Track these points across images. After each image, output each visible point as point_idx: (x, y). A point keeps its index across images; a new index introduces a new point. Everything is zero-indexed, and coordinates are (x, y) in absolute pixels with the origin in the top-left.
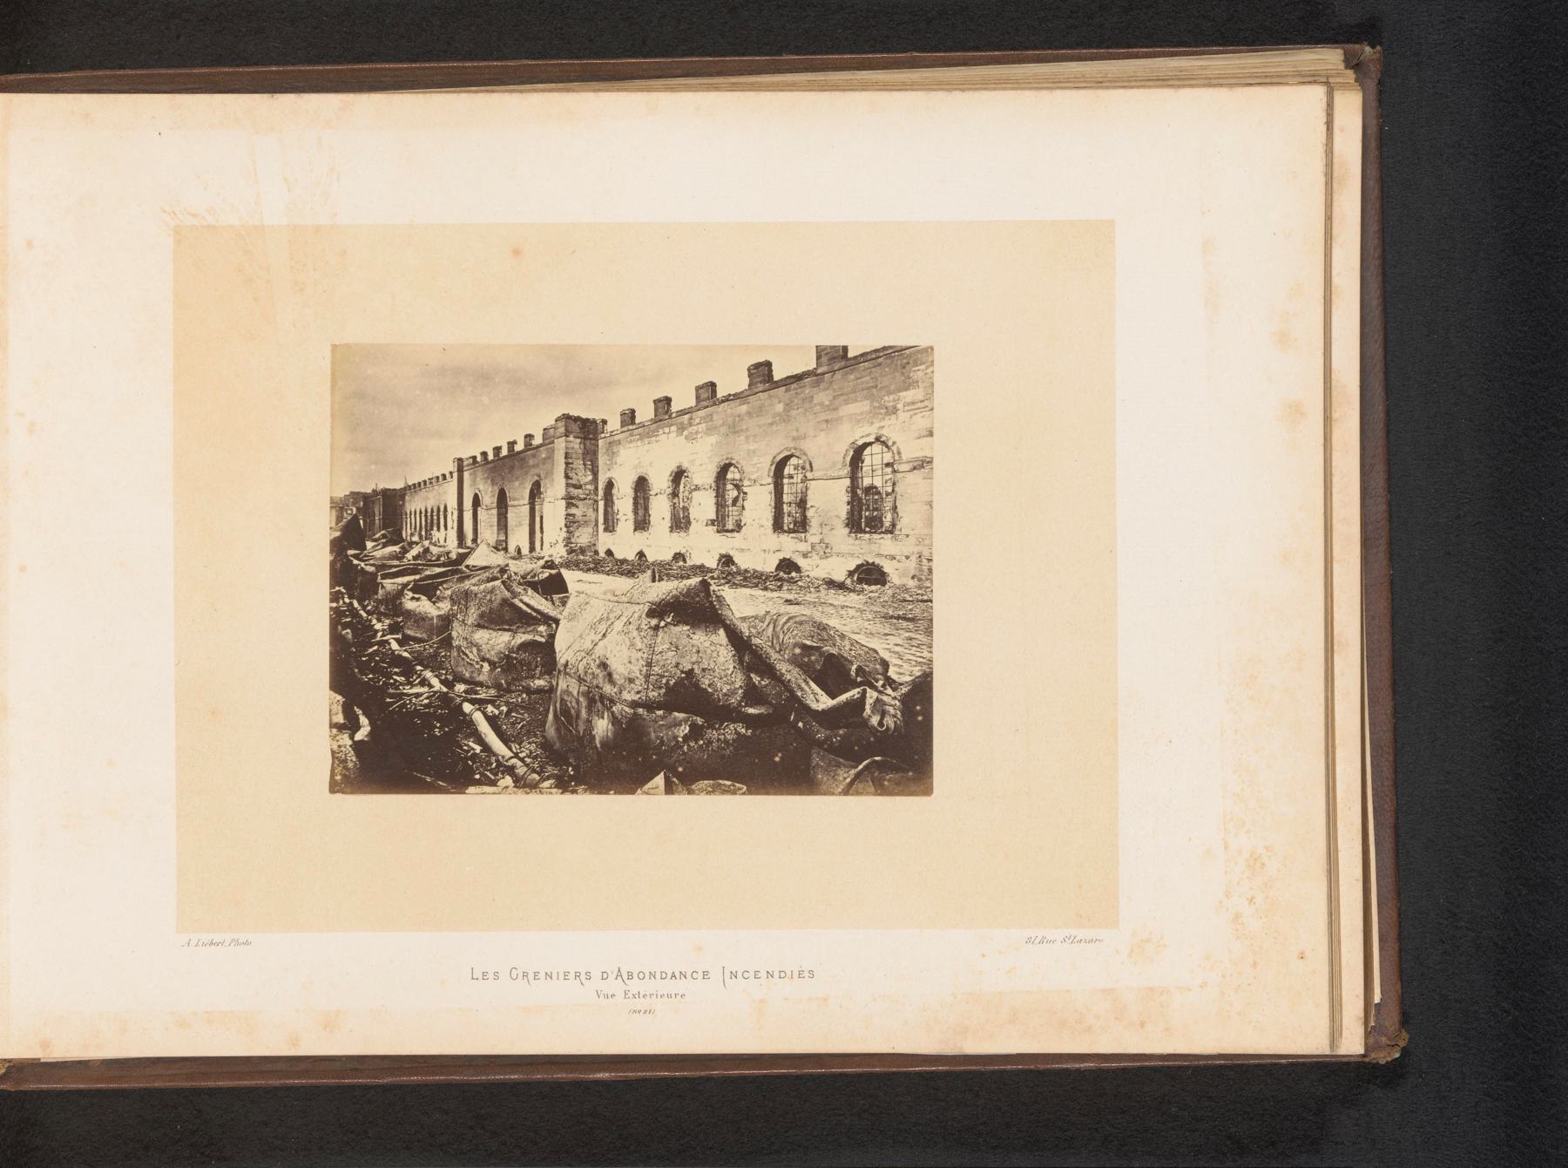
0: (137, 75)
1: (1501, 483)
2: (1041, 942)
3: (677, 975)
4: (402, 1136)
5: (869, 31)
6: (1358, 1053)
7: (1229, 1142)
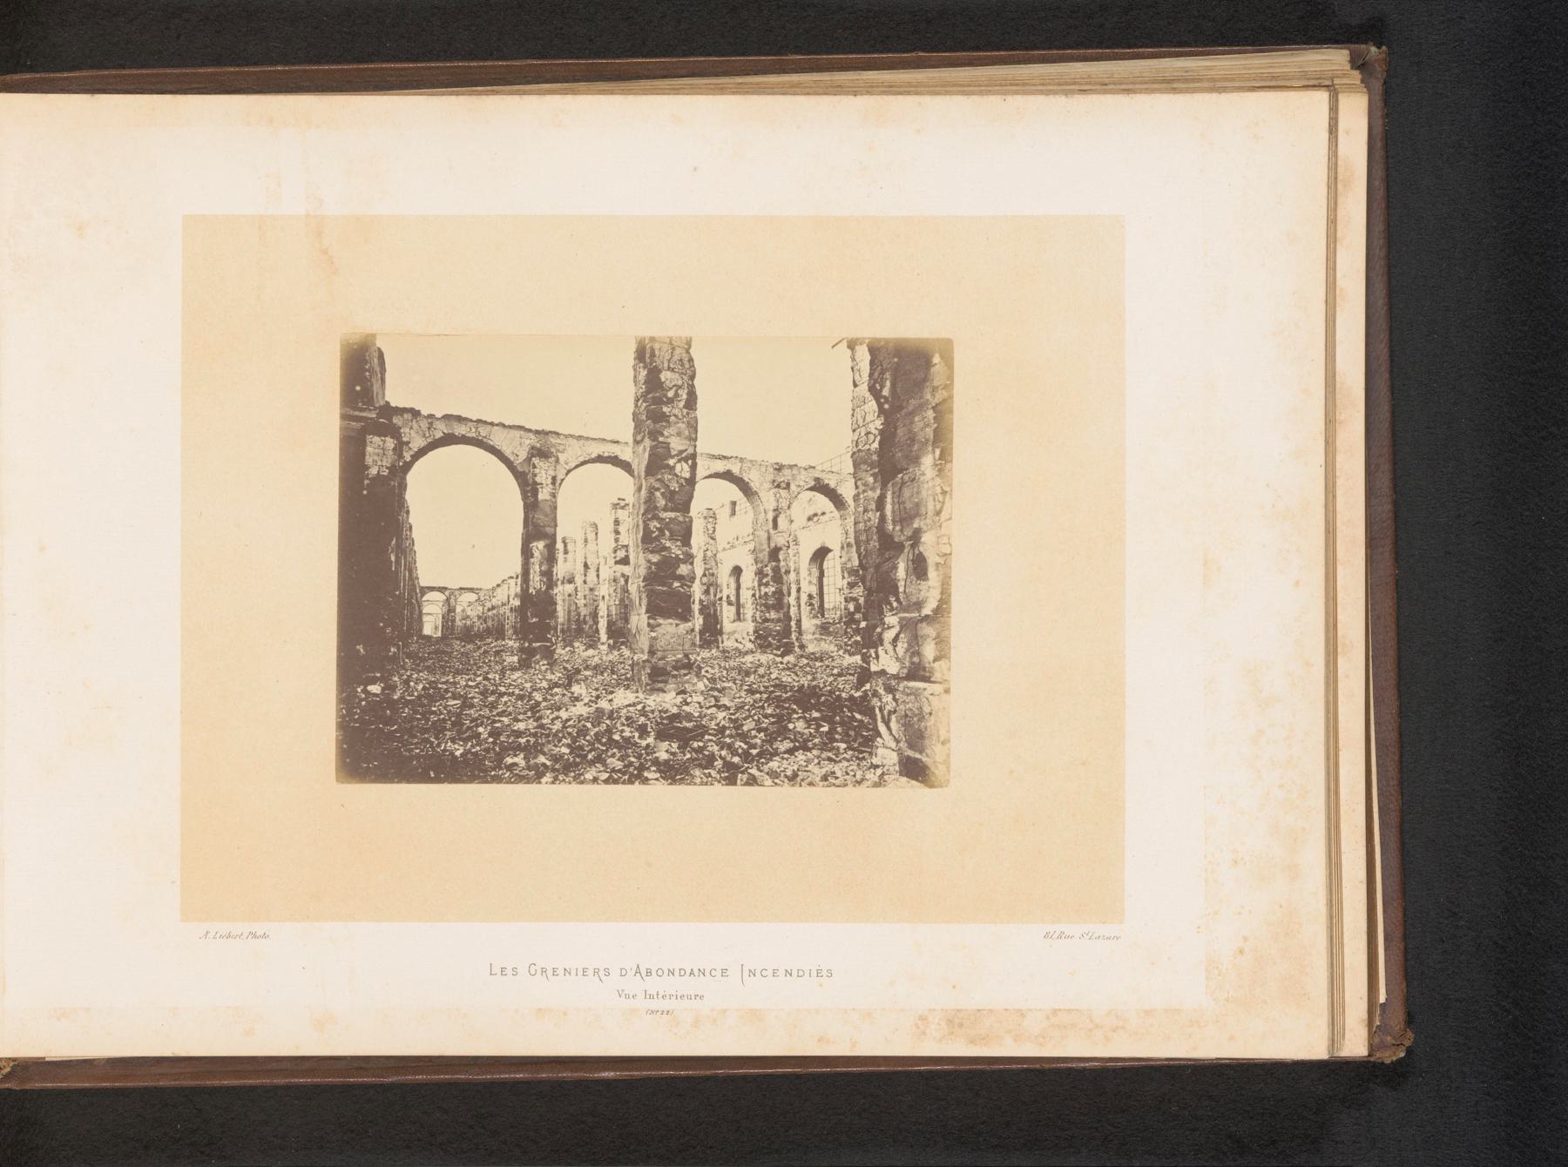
0: (143, 74)
1: (1501, 483)
2: (1060, 937)
3: (696, 972)
4: (402, 1135)
5: (869, 31)
6: (1361, 1055)
7: (1229, 1141)
